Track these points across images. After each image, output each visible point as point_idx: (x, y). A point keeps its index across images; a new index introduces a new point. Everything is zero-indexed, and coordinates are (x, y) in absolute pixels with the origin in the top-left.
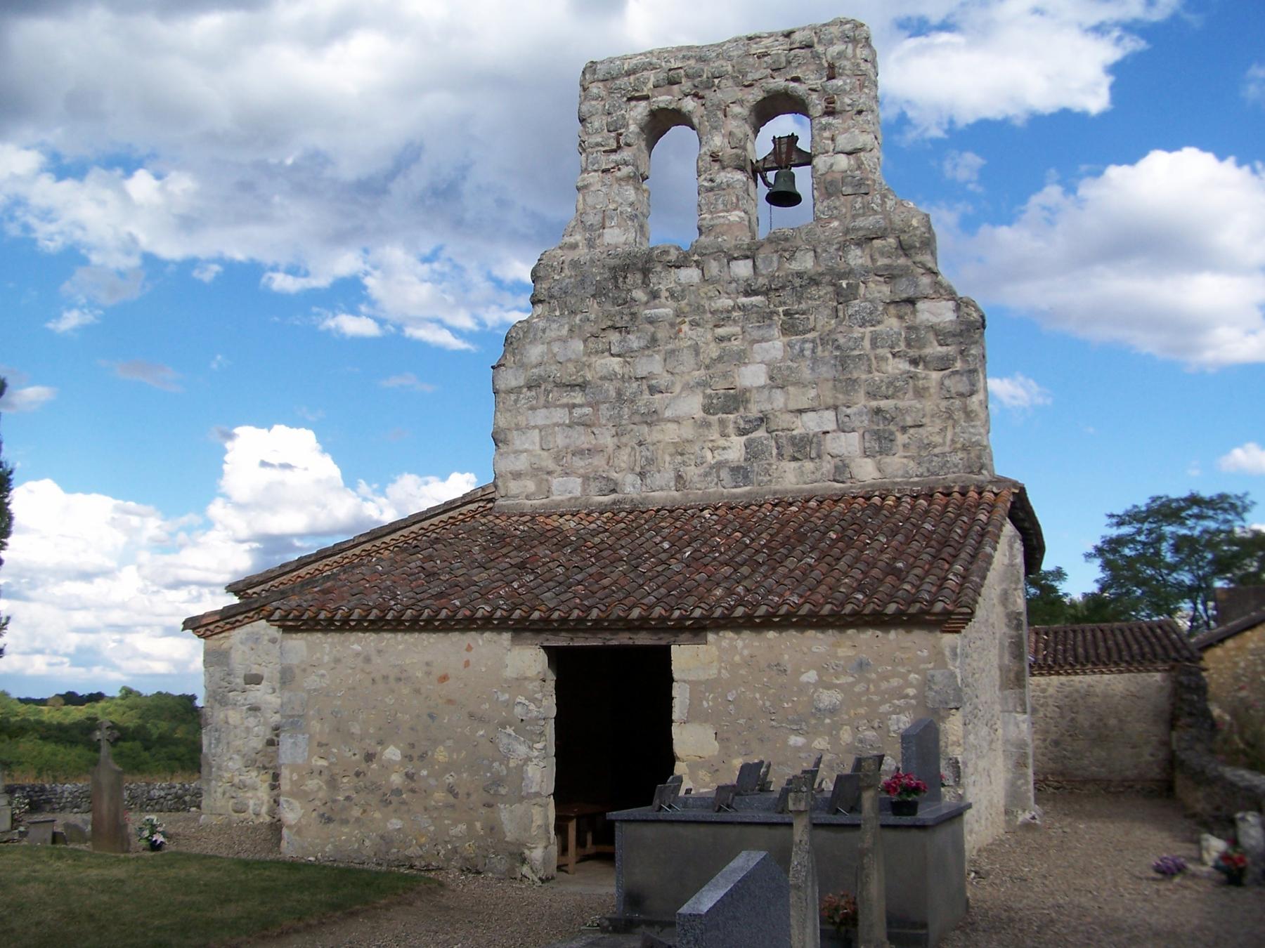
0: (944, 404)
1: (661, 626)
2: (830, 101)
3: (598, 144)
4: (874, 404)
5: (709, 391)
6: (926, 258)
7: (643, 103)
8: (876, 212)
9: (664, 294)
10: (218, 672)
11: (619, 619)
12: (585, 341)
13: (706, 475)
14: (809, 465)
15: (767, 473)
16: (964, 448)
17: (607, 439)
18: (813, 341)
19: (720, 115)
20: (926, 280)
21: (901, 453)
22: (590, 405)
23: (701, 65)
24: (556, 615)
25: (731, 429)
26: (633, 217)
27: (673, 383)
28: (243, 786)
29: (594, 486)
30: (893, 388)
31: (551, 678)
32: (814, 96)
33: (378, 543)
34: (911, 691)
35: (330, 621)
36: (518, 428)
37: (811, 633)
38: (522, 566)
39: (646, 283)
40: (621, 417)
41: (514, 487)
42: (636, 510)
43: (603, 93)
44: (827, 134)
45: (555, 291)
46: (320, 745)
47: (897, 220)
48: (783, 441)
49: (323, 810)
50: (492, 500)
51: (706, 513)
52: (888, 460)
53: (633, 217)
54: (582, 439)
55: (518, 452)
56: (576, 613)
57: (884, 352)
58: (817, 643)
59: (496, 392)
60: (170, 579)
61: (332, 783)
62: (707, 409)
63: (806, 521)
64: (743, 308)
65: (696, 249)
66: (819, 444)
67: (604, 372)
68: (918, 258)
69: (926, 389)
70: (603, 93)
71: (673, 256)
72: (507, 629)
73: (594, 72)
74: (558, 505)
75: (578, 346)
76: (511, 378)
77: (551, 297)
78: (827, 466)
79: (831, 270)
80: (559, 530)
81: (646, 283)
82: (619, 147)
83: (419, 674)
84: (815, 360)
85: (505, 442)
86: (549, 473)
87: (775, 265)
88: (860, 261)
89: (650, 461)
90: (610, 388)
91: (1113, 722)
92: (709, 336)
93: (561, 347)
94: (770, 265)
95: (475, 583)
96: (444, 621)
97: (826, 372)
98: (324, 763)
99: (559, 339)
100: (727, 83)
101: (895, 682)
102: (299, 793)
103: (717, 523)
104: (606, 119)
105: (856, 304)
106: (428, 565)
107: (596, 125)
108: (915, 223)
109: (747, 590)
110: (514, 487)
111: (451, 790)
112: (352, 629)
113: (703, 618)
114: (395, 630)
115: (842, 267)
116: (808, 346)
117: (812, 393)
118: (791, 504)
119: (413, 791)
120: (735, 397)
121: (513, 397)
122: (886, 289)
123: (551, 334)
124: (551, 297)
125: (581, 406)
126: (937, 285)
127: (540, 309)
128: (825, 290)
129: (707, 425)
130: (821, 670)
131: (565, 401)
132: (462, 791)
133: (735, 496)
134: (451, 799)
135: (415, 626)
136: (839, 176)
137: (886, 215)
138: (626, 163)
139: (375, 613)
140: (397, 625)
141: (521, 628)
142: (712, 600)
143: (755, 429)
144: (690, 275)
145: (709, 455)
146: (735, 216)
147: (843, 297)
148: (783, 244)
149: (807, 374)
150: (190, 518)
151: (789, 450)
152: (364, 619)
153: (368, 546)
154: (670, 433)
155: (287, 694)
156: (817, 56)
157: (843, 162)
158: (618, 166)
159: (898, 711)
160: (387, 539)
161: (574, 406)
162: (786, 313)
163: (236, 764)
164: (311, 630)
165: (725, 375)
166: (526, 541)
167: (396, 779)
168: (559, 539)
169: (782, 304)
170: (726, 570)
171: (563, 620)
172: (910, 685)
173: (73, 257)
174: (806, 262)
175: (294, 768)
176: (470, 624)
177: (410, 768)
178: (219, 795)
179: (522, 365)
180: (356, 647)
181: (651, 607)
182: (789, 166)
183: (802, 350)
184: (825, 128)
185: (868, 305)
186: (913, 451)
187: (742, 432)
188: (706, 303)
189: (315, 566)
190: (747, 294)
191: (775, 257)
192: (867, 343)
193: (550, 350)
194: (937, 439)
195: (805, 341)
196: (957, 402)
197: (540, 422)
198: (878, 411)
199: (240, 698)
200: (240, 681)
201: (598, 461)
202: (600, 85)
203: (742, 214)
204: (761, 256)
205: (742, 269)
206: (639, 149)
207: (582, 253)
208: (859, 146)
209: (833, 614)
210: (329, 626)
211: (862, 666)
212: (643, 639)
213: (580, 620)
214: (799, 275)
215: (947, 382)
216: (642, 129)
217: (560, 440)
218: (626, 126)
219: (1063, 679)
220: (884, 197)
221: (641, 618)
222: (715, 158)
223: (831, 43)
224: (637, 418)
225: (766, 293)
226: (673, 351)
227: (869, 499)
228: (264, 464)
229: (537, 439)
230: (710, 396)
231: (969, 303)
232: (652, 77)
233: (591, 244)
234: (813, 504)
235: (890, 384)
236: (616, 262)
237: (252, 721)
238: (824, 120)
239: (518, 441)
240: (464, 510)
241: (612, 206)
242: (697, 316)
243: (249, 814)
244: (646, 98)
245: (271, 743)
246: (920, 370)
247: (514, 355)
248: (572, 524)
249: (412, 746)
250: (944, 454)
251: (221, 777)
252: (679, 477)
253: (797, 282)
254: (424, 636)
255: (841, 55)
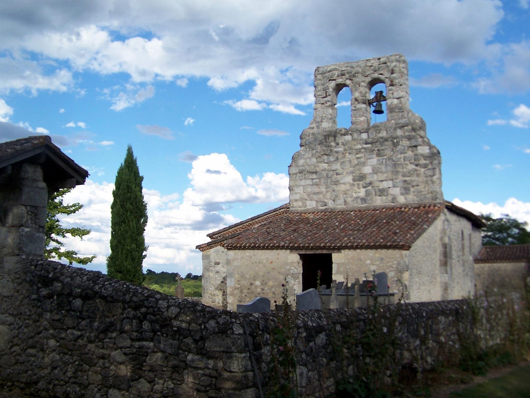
0: (425, 179)
1: (329, 248)
2: (392, 81)
3: (320, 95)
4: (404, 179)
5: (354, 175)
6: (422, 133)
7: (334, 82)
8: (405, 118)
9: (341, 144)
10: (207, 261)
11: (318, 246)
12: (317, 158)
13: (353, 200)
14: (384, 198)
15: (372, 200)
16: (431, 193)
17: (323, 189)
18: (386, 159)
19: (358, 86)
20: (420, 140)
21: (412, 194)
22: (318, 179)
23: (351, 69)
24: (301, 245)
25: (361, 186)
26: (331, 119)
27: (343, 172)
28: (214, 295)
29: (319, 204)
30: (410, 174)
31: (301, 262)
32: (387, 80)
33: (254, 221)
34: (395, 266)
35: (240, 247)
36: (296, 186)
37: (369, 250)
38: (294, 230)
39: (335, 140)
40: (327, 182)
41: (295, 204)
42: (332, 211)
43: (321, 78)
44: (391, 92)
45: (307, 143)
46: (238, 281)
47: (412, 120)
48: (377, 190)
49: (239, 299)
50: (289, 208)
51: (352, 213)
52: (408, 196)
53: (331, 119)
54: (316, 189)
55: (296, 193)
56: (307, 245)
57: (407, 162)
58: (370, 253)
59: (289, 174)
60: (167, 223)
61: (241, 292)
62: (354, 180)
63: (380, 216)
64: (364, 148)
65: (350, 129)
66: (387, 191)
67: (322, 168)
68: (419, 133)
69: (420, 174)
70: (321, 78)
71: (343, 132)
72: (288, 249)
73: (318, 71)
74: (309, 210)
75: (314, 160)
76: (294, 170)
77: (306, 144)
78: (390, 198)
79: (391, 137)
80: (307, 218)
81: (335, 140)
82: (326, 96)
83: (265, 261)
84: (386, 165)
85: (293, 190)
86: (306, 200)
87: (374, 135)
88: (400, 134)
89: (337, 196)
90: (324, 173)
91: (507, 280)
92: (354, 157)
93: (308, 160)
94: (373, 135)
95: (281, 236)
96: (272, 247)
97: (390, 169)
98: (239, 286)
99: (308, 158)
100: (360, 75)
101: (390, 264)
102: (232, 294)
103: (354, 216)
104: (322, 87)
105: (399, 147)
106: (268, 230)
107: (319, 88)
108: (417, 121)
109: (354, 238)
110: (295, 204)
111: (274, 293)
112: (247, 249)
113: (340, 246)
114: (258, 249)
115: (395, 136)
116: (384, 160)
117: (385, 175)
118: (377, 210)
119: (263, 293)
120: (362, 177)
121: (295, 176)
122: (408, 143)
123: (306, 156)
124: (306, 144)
125: (315, 179)
126: (424, 141)
127: (303, 148)
128: (389, 143)
129: (353, 185)
130: (371, 260)
131: (310, 177)
132: (276, 293)
133: (362, 207)
134: (274, 295)
135: (264, 248)
136: (394, 106)
137: (409, 118)
138: (329, 101)
139: (253, 245)
140: (259, 248)
141: (292, 249)
142: (343, 241)
143: (368, 186)
144: (348, 138)
145: (354, 194)
146: (362, 119)
147: (395, 145)
148: (377, 128)
149: (384, 169)
150: (175, 196)
151: (378, 193)
152: (250, 246)
153: (250, 222)
154: (342, 188)
155: (229, 267)
156: (388, 67)
157: (396, 101)
158: (326, 102)
159: (391, 271)
160: (256, 220)
161: (313, 179)
162: (378, 150)
163: (212, 288)
164: (235, 249)
165: (359, 170)
166: (298, 222)
167: (259, 290)
168: (306, 221)
169: (376, 147)
170: (351, 232)
171: (303, 247)
172: (394, 264)
173: (122, 78)
174: (384, 134)
175: (231, 287)
176: (278, 248)
177: (262, 287)
178: (207, 297)
179: (297, 166)
180: (248, 254)
181: (326, 243)
182: (380, 101)
183: (382, 162)
184: (390, 90)
185: (402, 147)
186: (416, 193)
187: (364, 187)
188: (354, 147)
189: (234, 228)
190: (366, 144)
191: (374, 132)
192: (402, 160)
193: (306, 161)
194: (423, 190)
195: (383, 159)
196: (429, 178)
197: (303, 184)
198: (405, 181)
199: (213, 269)
200: (213, 264)
201: (321, 196)
202: (320, 75)
203: (365, 118)
204: (370, 132)
205: (364, 136)
206: (333, 96)
207: (315, 130)
208: (400, 96)
209: (373, 245)
210: (240, 248)
211: (382, 259)
212: (325, 252)
213: (307, 247)
214: (382, 138)
215: (426, 172)
216: (334, 90)
217: (309, 189)
218: (328, 89)
219: (490, 265)
220: (408, 113)
221: (323, 246)
222: (356, 100)
223: (392, 62)
224: (332, 183)
225: (371, 143)
226: (343, 162)
227: (401, 208)
228: (208, 171)
229: (302, 189)
230: (354, 176)
231: (434, 147)
232: (336, 73)
233: (318, 127)
234: (384, 210)
235: (409, 172)
236: (326, 133)
237: (217, 276)
238: (390, 88)
239: (297, 190)
240: (280, 211)
241: (324, 115)
242: (350, 150)
243: (216, 303)
244: (335, 80)
245: (222, 282)
246: (418, 168)
247: (295, 162)
248: (312, 216)
249: (263, 281)
250: (425, 194)
251: (208, 292)
252: (345, 201)
253: (381, 140)
254: (266, 251)
255: (395, 66)
